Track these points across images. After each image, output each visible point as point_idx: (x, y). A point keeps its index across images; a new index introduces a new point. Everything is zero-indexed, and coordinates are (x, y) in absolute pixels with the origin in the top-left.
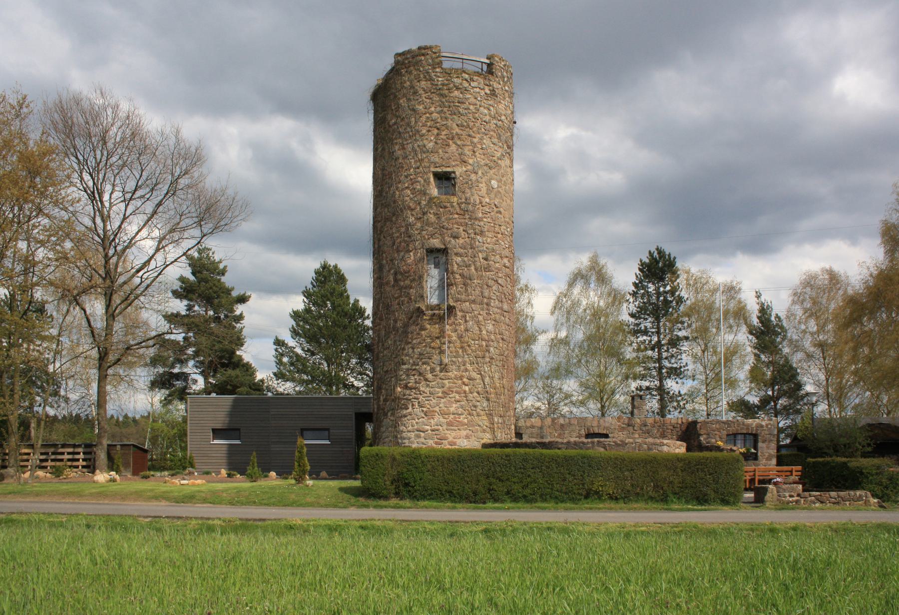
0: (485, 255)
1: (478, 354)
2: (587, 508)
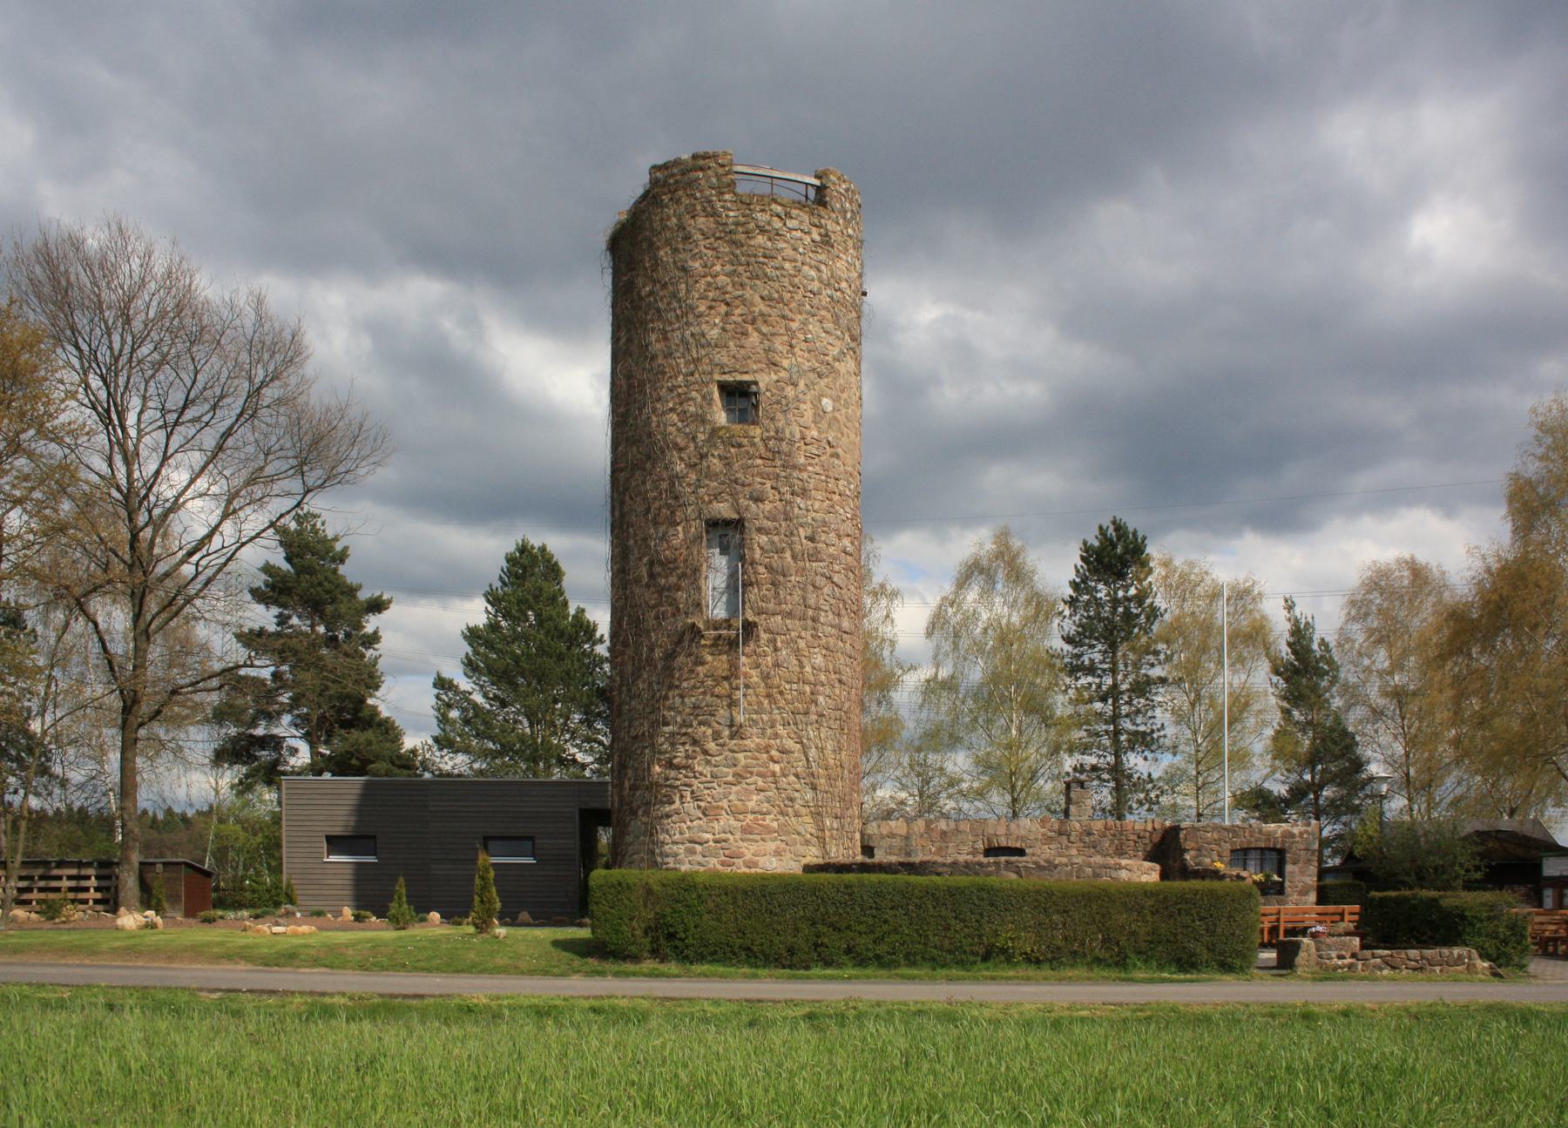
2: (986, 978)
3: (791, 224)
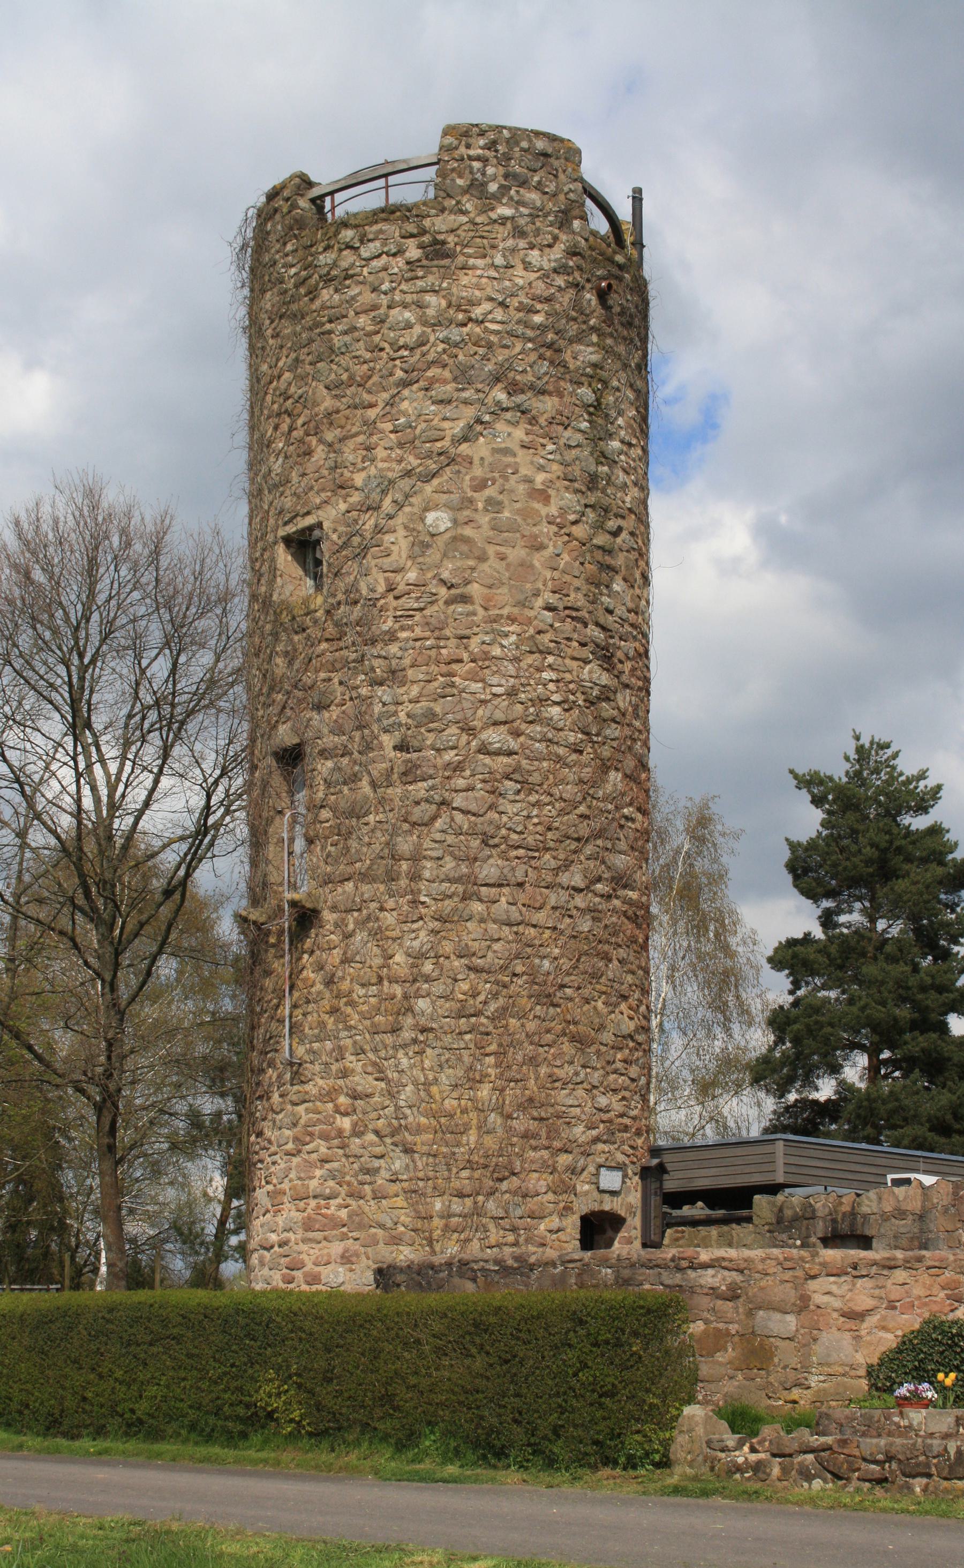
3: (365, 253)
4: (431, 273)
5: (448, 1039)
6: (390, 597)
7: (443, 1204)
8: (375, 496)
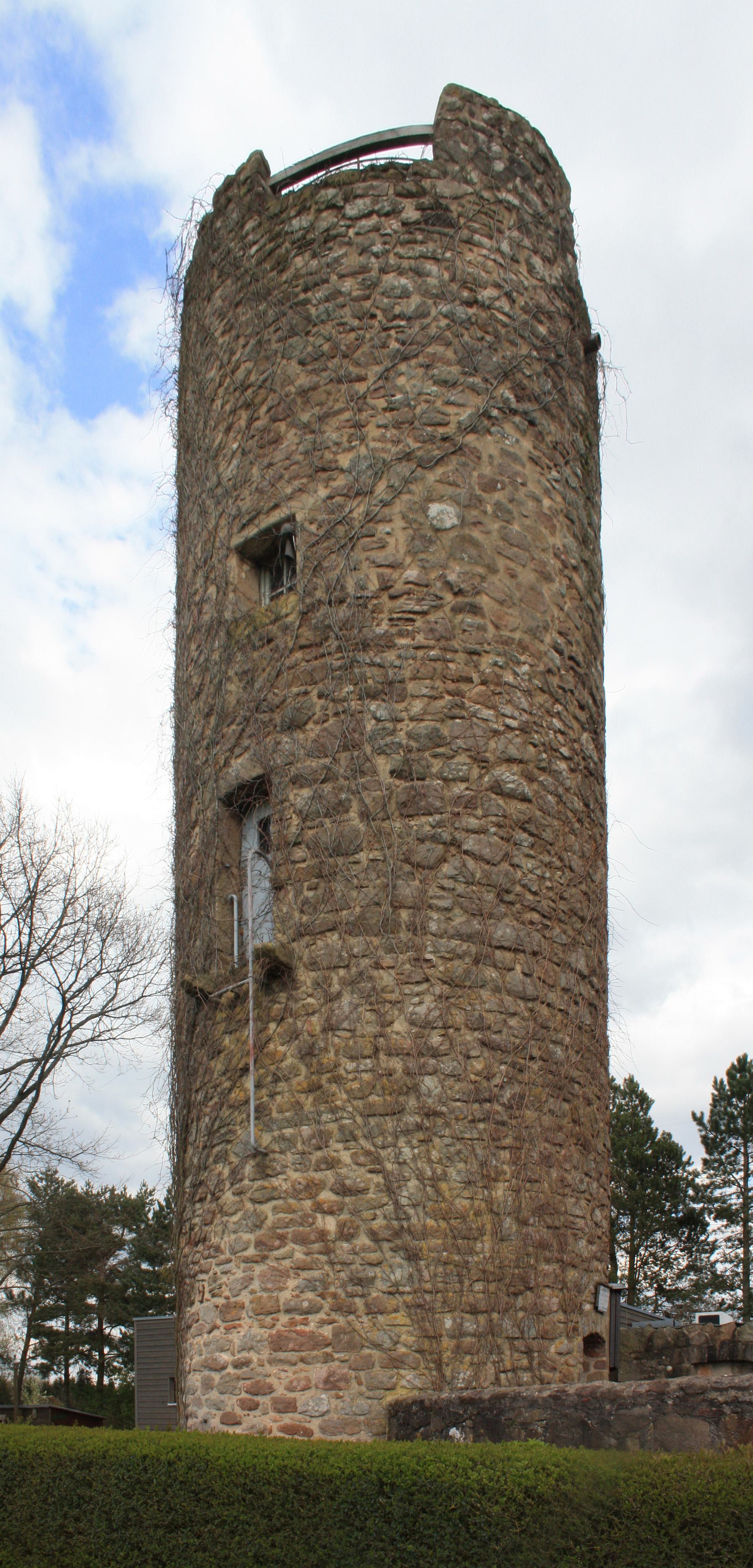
0: (397, 758)
1: (371, 1105)
3: (351, 210)
4: (432, 239)
5: (458, 1127)
6: (385, 598)
7: (454, 1320)
8: (366, 479)
